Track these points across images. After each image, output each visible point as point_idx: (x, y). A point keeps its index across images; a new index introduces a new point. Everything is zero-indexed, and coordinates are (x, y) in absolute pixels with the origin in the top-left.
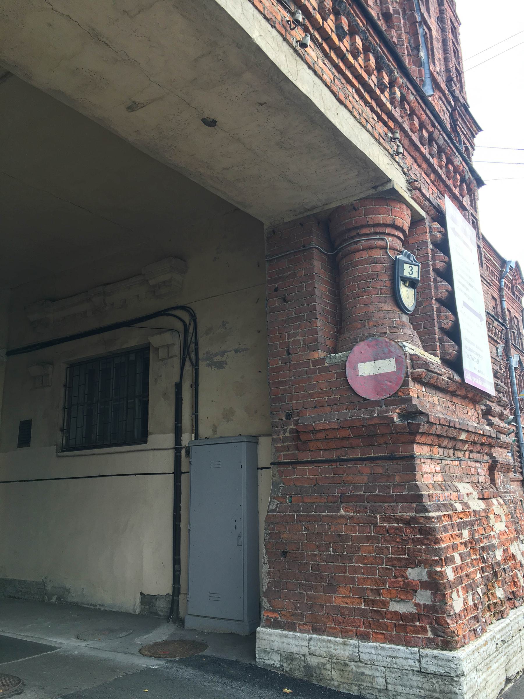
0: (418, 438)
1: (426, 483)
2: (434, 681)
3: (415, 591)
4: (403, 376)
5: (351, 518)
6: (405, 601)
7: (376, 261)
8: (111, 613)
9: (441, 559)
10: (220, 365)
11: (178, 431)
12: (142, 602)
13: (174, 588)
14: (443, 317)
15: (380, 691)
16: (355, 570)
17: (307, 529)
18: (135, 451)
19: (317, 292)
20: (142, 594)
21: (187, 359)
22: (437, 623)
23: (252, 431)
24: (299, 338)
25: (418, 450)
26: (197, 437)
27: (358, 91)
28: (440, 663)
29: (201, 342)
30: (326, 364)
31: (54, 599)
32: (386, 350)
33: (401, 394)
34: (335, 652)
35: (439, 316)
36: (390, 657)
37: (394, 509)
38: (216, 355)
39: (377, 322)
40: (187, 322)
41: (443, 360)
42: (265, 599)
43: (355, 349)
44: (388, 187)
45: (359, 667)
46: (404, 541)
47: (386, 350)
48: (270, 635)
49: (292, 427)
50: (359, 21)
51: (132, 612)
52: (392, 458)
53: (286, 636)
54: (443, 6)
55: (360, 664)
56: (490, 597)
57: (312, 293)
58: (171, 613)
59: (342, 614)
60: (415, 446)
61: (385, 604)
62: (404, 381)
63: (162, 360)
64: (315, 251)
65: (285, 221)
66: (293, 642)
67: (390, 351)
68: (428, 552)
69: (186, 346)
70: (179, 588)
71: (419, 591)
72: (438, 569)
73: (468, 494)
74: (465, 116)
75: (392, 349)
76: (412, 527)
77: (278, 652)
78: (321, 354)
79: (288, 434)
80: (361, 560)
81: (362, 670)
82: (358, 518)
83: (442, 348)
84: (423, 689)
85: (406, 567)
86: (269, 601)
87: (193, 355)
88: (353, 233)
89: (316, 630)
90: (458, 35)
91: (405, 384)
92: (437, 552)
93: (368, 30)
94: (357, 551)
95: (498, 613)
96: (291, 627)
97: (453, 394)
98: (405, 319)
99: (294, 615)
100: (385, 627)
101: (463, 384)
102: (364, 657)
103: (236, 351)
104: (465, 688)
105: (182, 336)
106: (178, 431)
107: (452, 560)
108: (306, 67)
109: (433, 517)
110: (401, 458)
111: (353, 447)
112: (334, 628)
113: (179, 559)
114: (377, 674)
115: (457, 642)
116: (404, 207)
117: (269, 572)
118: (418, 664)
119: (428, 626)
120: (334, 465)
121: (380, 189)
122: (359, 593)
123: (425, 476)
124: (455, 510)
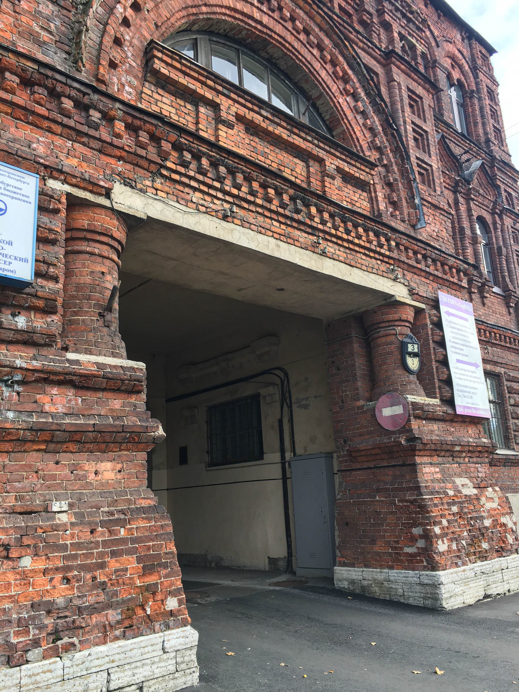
0: (417, 453)
1: (426, 479)
2: (427, 588)
3: (417, 540)
4: (407, 416)
5: (382, 501)
6: (412, 546)
7: (391, 343)
8: (250, 570)
9: (431, 522)
10: (306, 407)
11: (283, 451)
12: (269, 563)
13: (288, 553)
14: (440, 373)
15: (400, 596)
16: (385, 531)
17: (358, 509)
18: (256, 465)
19: (357, 364)
20: (269, 557)
21: (285, 403)
22: (428, 557)
23: (329, 449)
24: (348, 393)
25: (418, 460)
26: (294, 455)
27: (365, 254)
28: (429, 578)
29: (293, 391)
30: (365, 409)
31: (213, 565)
32: (397, 400)
33: (407, 427)
34: (376, 577)
35: (437, 372)
36: (404, 577)
37: (405, 495)
38: (303, 400)
39: (393, 382)
40: (283, 378)
41: (441, 400)
42: (337, 551)
43: (380, 400)
44: (393, 299)
45: (389, 584)
46: (411, 513)
47: (397, 400)
48: (341, 570)
49: (348, 448)
50: (359, 221)
51: (263, 569)
52: (404, 465)
53: (350, 570)
54: (478, 78)
55: (389, 583)
56: (477, 547)
57: (354, 365)
58: (288, 568)
59: (379, 556)
60: (416, 458)
61: (402, 549)
62: (408, 419)
63: (268, 404)
64: (354, 338)
65: (335, 319)
66: (353, 573)
67: (399, 401)
68: (423, 518)
69: (283, 395)
70: (291, 552)
71: (419, 540)
72: (429, 528)
73: (463, 485)
74: (504, 169)
75: (401, 400)
76: (415, 505)
77: (346, 580)
78: (361, 403)
79: (345, 453)
80: (388, 525)
81: (391, 586)
82: (386, 501)
83: (441, 393)
84: (422, 593)
85: (412, 527)
86: (340, 552)
87: (288, 400)
88: (376, 327)
89: (366, 566)
90: (496, 96)
91: (409, 420)
92: (428, 518)
93: (366, 222)
94: (386, 520)
95: (483, 557)
96: (353, 565)
97: (452, 421)
98: (413, 378)
99: (354, 558)
100: (402, 561)
101: (456, 415)
102: (392, 578)
103: (315, 397)
104: (443, 591)
105: (280, 387)
106: (283, 451)
107: (440, 523)
108: (328, 259)
109: (426, 499)
110: (409, 465)
111: (382, 460)
112: (376, 564)
113: (290, 534)
114: (398, 587)
115: (439, 567)
116: (408, 307)
117: (339, 535)
118: (419, 580)
119: (424, 559)
120: (373, 470)
121: (388, 300)
122: (388, 543)
123: (425, 475)
124: (446, 494)
